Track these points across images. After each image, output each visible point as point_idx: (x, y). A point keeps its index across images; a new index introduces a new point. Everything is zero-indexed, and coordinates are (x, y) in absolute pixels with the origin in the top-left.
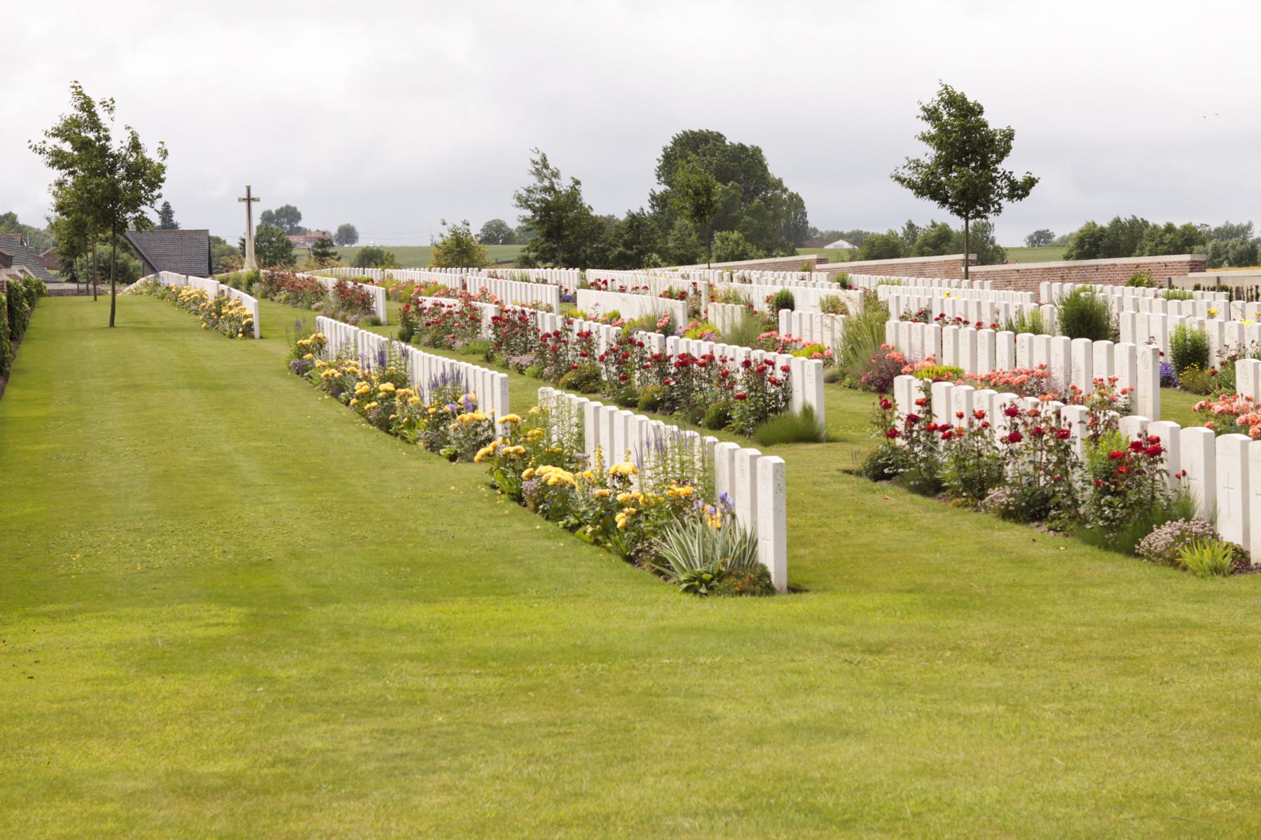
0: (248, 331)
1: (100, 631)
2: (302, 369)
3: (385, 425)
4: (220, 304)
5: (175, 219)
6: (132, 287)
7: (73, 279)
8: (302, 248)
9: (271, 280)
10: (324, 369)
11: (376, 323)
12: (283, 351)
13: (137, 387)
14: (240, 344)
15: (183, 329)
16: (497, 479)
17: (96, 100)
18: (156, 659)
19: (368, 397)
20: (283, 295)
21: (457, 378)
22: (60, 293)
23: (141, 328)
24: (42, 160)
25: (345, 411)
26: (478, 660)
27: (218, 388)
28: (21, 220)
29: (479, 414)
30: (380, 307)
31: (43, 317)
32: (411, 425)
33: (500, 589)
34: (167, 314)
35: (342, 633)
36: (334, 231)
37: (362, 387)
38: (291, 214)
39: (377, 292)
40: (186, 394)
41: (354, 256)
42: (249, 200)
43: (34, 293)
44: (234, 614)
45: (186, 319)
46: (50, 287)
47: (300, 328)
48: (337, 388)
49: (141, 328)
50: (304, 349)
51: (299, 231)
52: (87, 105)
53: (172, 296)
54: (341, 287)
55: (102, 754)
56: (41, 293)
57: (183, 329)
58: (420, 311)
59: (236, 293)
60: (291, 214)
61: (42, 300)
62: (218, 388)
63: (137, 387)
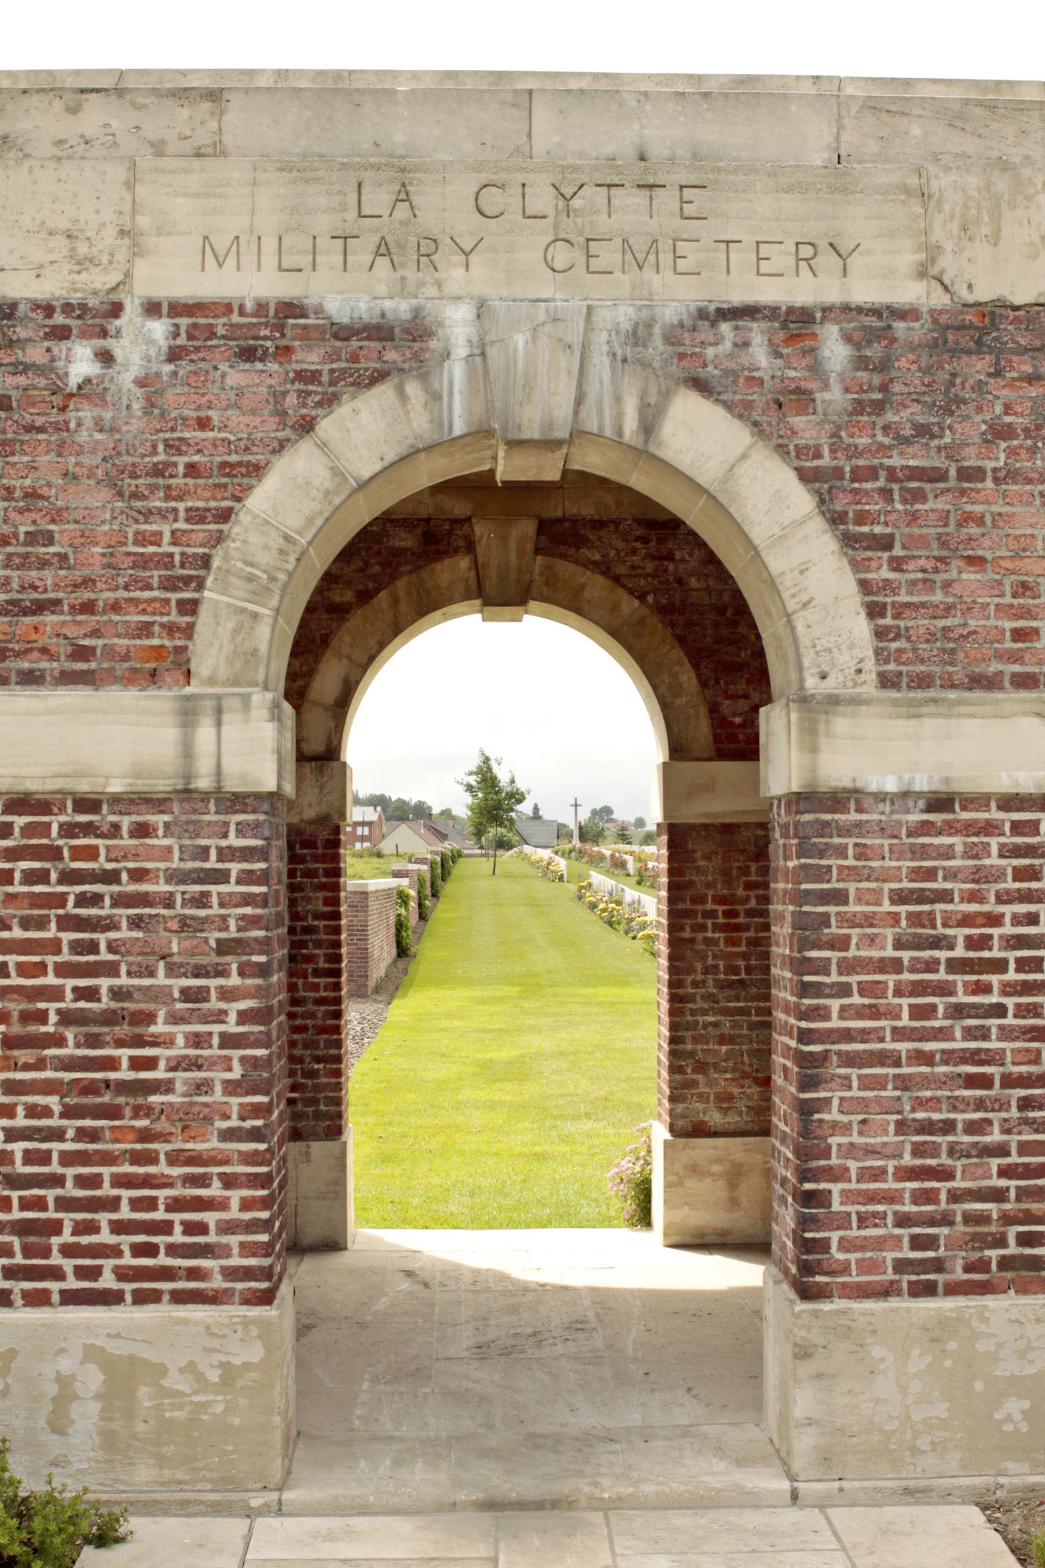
0: (561, 878)
1: (464, 993)
3: (610, 924)
4: (549, 864)
5: (541, 813)
6: (511, 852)
7: (482, 848)
8: (611, 830)
9: (580, 851)
10: (589, 898)
11: (628, 875)
12: (573, 888)
14: (557, 884)
16: (646, 946)
17: (492, 757)
18: (483, 1001)
19: (604, 910)
20: (585, 859)
21: (639, 902)
22: (472, 856)
23: (509, 876)
25: (595, 918)
28: (454, 813)
30: (631, 866)
31: (459, 869)
32: (619, 923)
33: (627, 984)
34: (525, 868)
35: (555, 995)
36: (632, 821)
37: (602, 906)
38: (607, 811)
39: (629, 859)
42: (576, 805)
43: (456, 856)
44: (516, 989)
46: (466, 852)
47: (581, 877)
48: (593, 906)
49: (509, 876)
50: (582, 887)
51: (612, 820)
52: (487, 760)
53: (526, 858)
54: (612, 856)
55: (457, 1023)
56: (460, 855)
57: (527, 876)
58: (646, 869)
59: (557, 858)
60: (607, 811)
61: (461, 860)
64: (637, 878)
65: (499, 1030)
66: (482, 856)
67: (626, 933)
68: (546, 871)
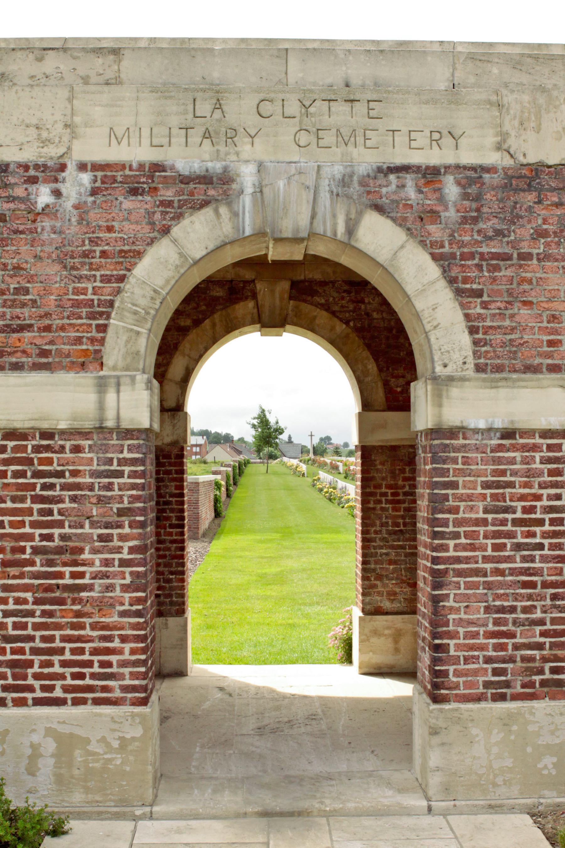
1: (251, 537)
2: (314, 485)
3: (330, 500)
4: (297, 467)
5: (292, 440)
6: (276, 461)
7: (260, 458)
9: (314, 460)
12: (310, 480)
13: (270, 489)
14: (301, 478)
15: (285, 474)
16: (349, 512)
17: (266, 409)
18: (261, 542)
19: (327, 492)
20: (316, 465)
22: (255, 463)
23: (275, 473)
24: (249, 427)
25: (321, 496)
26: (325, 543)
27: (291, 490)
29: (349, 497)
30: (341, 469)
31: (248, 470)
32: (335, 499)
36: (342, 444)
37: (325, 490)
38: (328, 438)
39: (340, 464)
40: (283, 491)
41: (347, 452)
42: (311, 436)
44: (279, 535)
45: (287, 471)
46: (252, 461)
47: (314, 474)
48: (321, 490)
49: (275, 473)
50: (314, 480)
51: (331, 444)
52: (263, 411)
53: (284, 464)
54: (331, 463)
55: (247, 553)
56: (249, 462)
57: (285, 474)
58: (349, 470)
60: (328, 438)
61: (249, 465)
62: (291, 490)
63: (270, 489)
64: (344, 475)
66: (260, 463)
67: (339, 504)
68: (295, 471)
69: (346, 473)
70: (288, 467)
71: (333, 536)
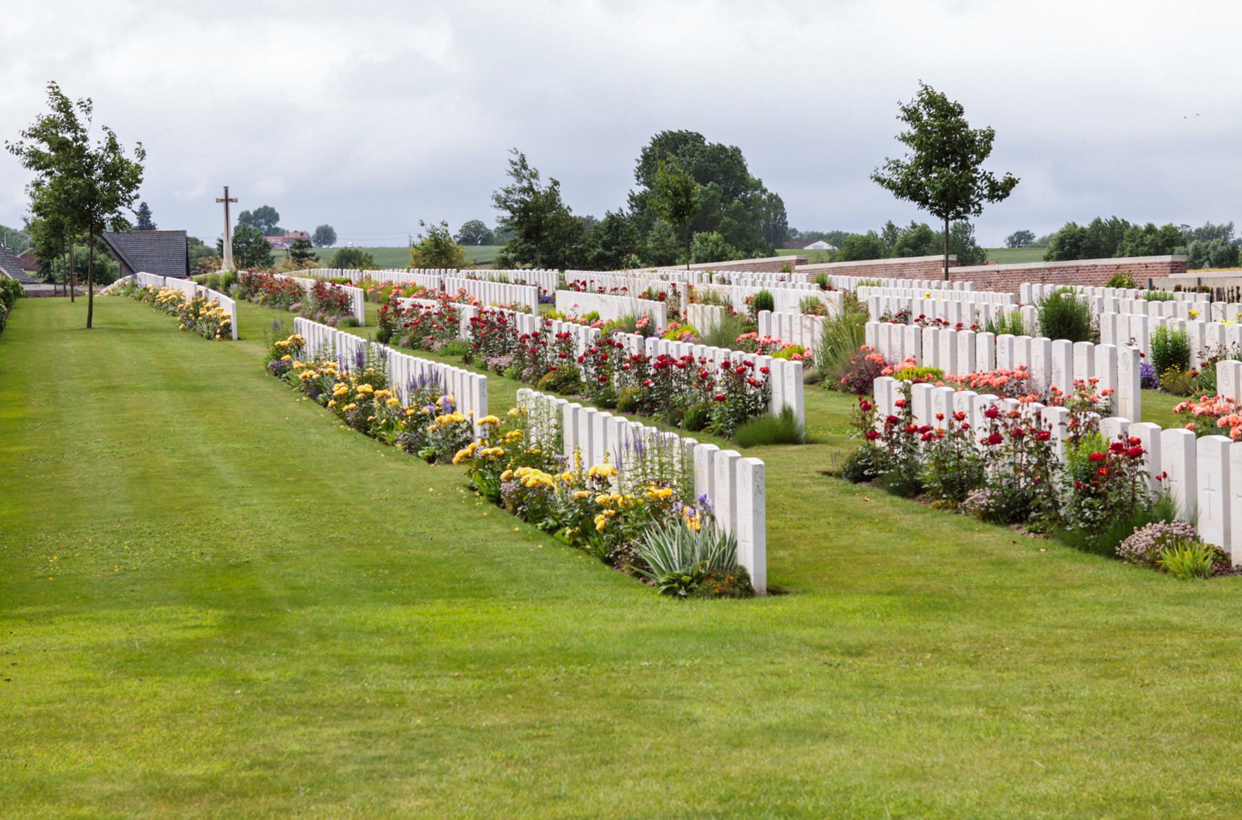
0: (226, 332)
1: (77, 634)
2: (280, 371)
3: (363, 426)
4: (197, 305)
5: (153, 220)
6: (109, 288)
7: (51, 280)
9: (249, 281)
10: (302, 370)
12: (260, 352)
13: (114, 389)
14: (217, 345)
15: (154, 330)
16: (475, 480)
17: (73, 100)
19: (346, 398)
20: (261, 296)
21: (435, 379)
22: (37, 294)
23: (120, 329)
24: (18, 161)
25: (323, 413)
26: (457, 662)
27: (196, 389)
29: (458, 416)
30: (359, 308)
33: (478, 591)
34: (143, 315)
35: (321, 636)
36: (312, 232)
39: (355, 293)
40: (164, 396)
42: (227, 200)
44: (211, 616)
46: (27, 288)
47: (279, 330)
48: (315, 389)
49: (120, 329)
51: (277, 232)
53: (149, 298)
54: (319, 288)
55: (80, 757)
57: (154, 330)
58: (398, 313)
61: (20, 301)
62: (196, 389)
63: (114, 389)
64: (376, 330)
65: (211, 785)
66: (57, 293)
67: (411, 448)
68: (193, 319)
69: (384, 322)
70: (161, 306)
71: (466, 613)
